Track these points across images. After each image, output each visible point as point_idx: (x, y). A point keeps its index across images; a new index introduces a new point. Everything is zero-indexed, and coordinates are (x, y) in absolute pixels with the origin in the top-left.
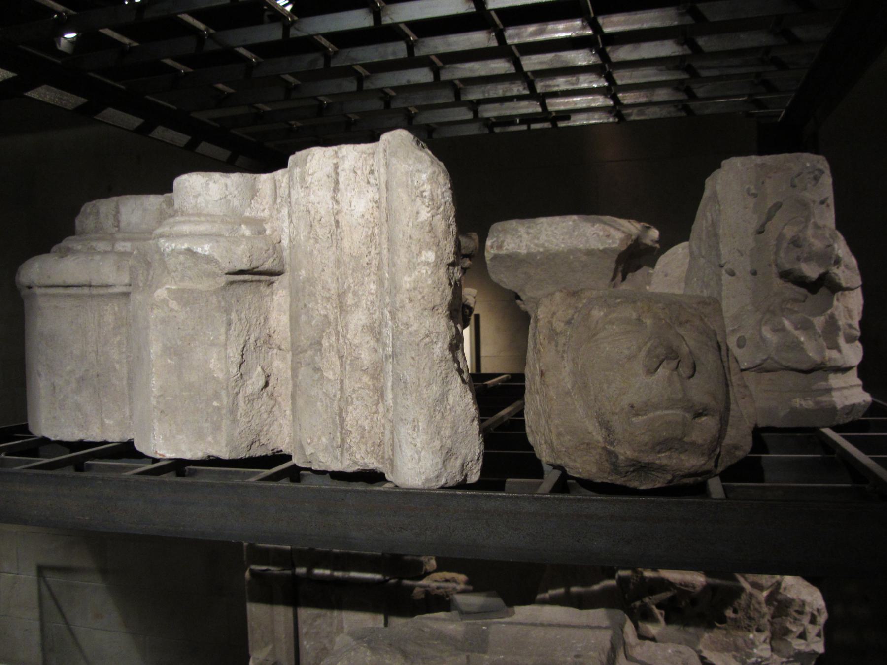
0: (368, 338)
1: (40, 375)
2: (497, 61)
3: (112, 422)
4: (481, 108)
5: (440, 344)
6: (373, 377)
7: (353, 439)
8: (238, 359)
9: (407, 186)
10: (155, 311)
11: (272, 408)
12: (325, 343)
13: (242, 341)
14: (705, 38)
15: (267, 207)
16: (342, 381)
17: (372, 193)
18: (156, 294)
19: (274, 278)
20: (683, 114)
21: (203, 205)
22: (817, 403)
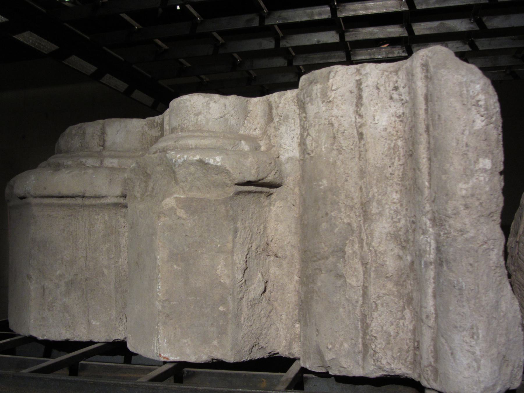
0: (392, 246)
1: (29, 277)
2: (392, 26)
3: (98, 323)
5: (496, 251)
6: (397, 284)
7: (379, 345)
8: (242, 265)
9: (461, 95)
10: (162, 219)
11: (270, 312)
12: (349, 250)
13: (246, 249)
15: (259, 126)
16: (365, 288)
17: (396, 108)
18: (164, 203)
19: (274, 190)
21: (204, 122)
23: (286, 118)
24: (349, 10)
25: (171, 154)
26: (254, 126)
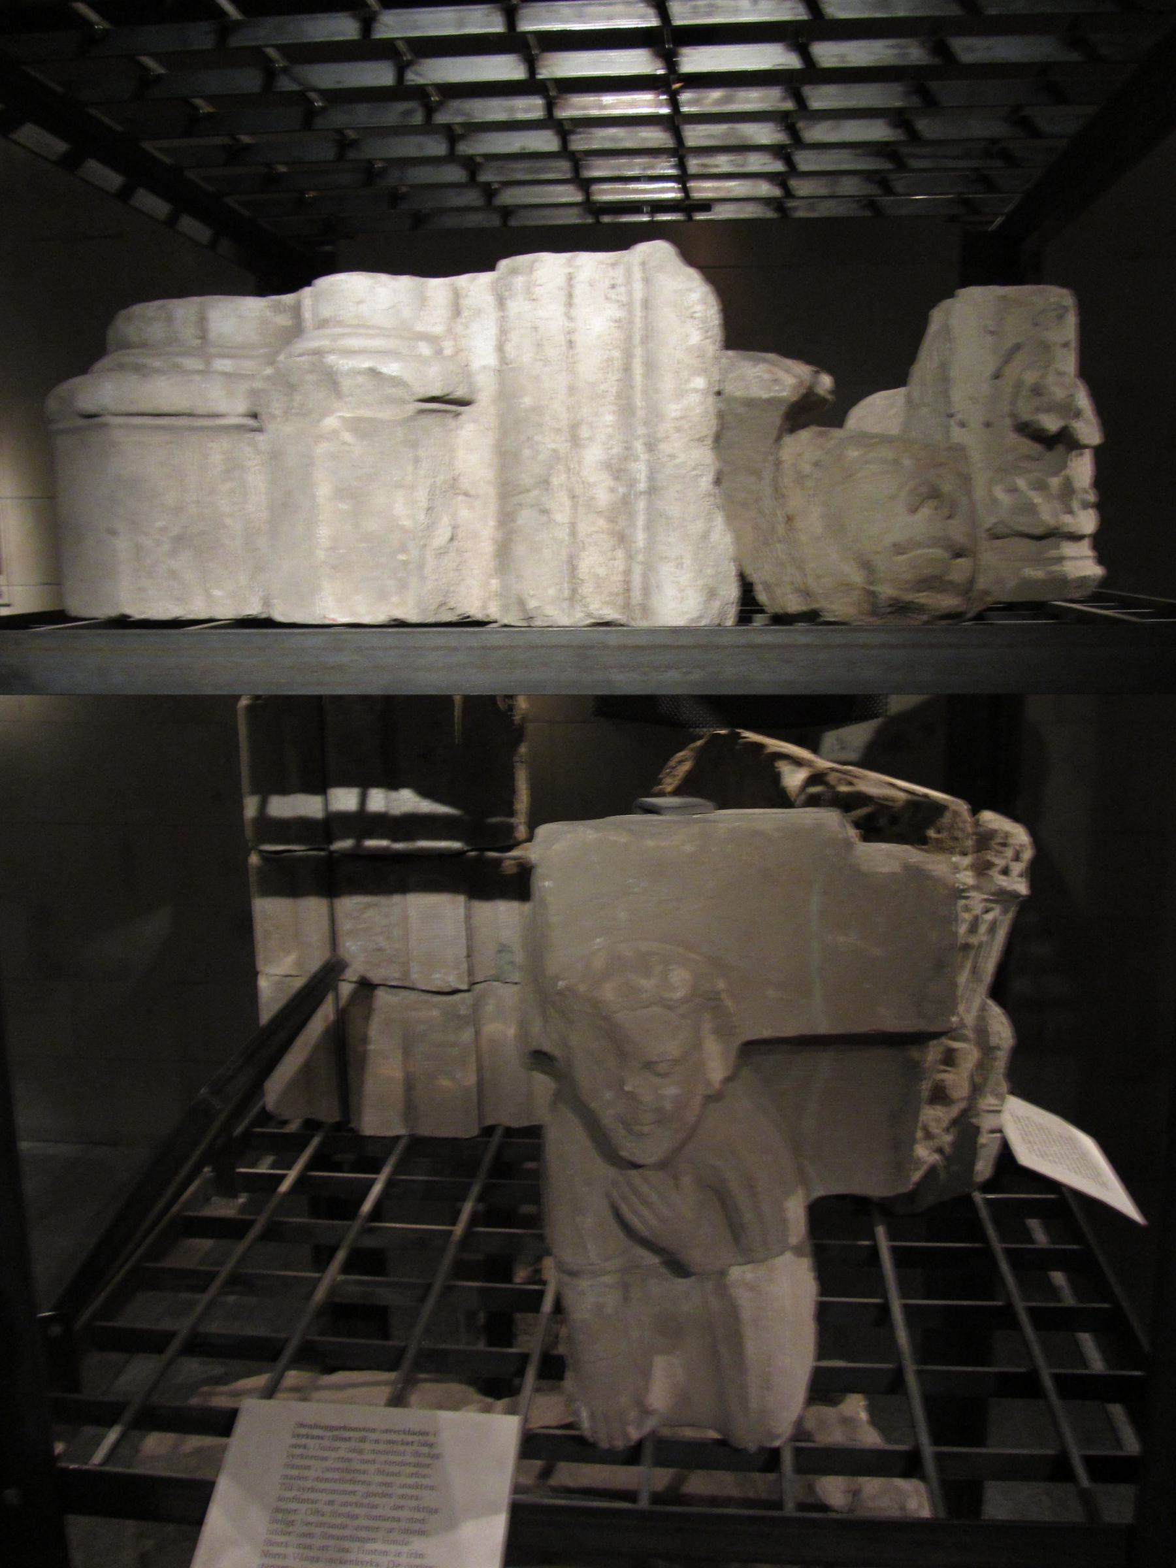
1: (113, 532)
2: (652, 128)
4: (595, 188)
6: (612, 520)
7: (587, 589)
12: (555, 481)
14: (925, 122)
16: (573, 525)
20: (868, 213)
22: (1050, 572)
23: (478, 312)
24: (574, 107)
25: (331, 359)
26: (435, 320)
